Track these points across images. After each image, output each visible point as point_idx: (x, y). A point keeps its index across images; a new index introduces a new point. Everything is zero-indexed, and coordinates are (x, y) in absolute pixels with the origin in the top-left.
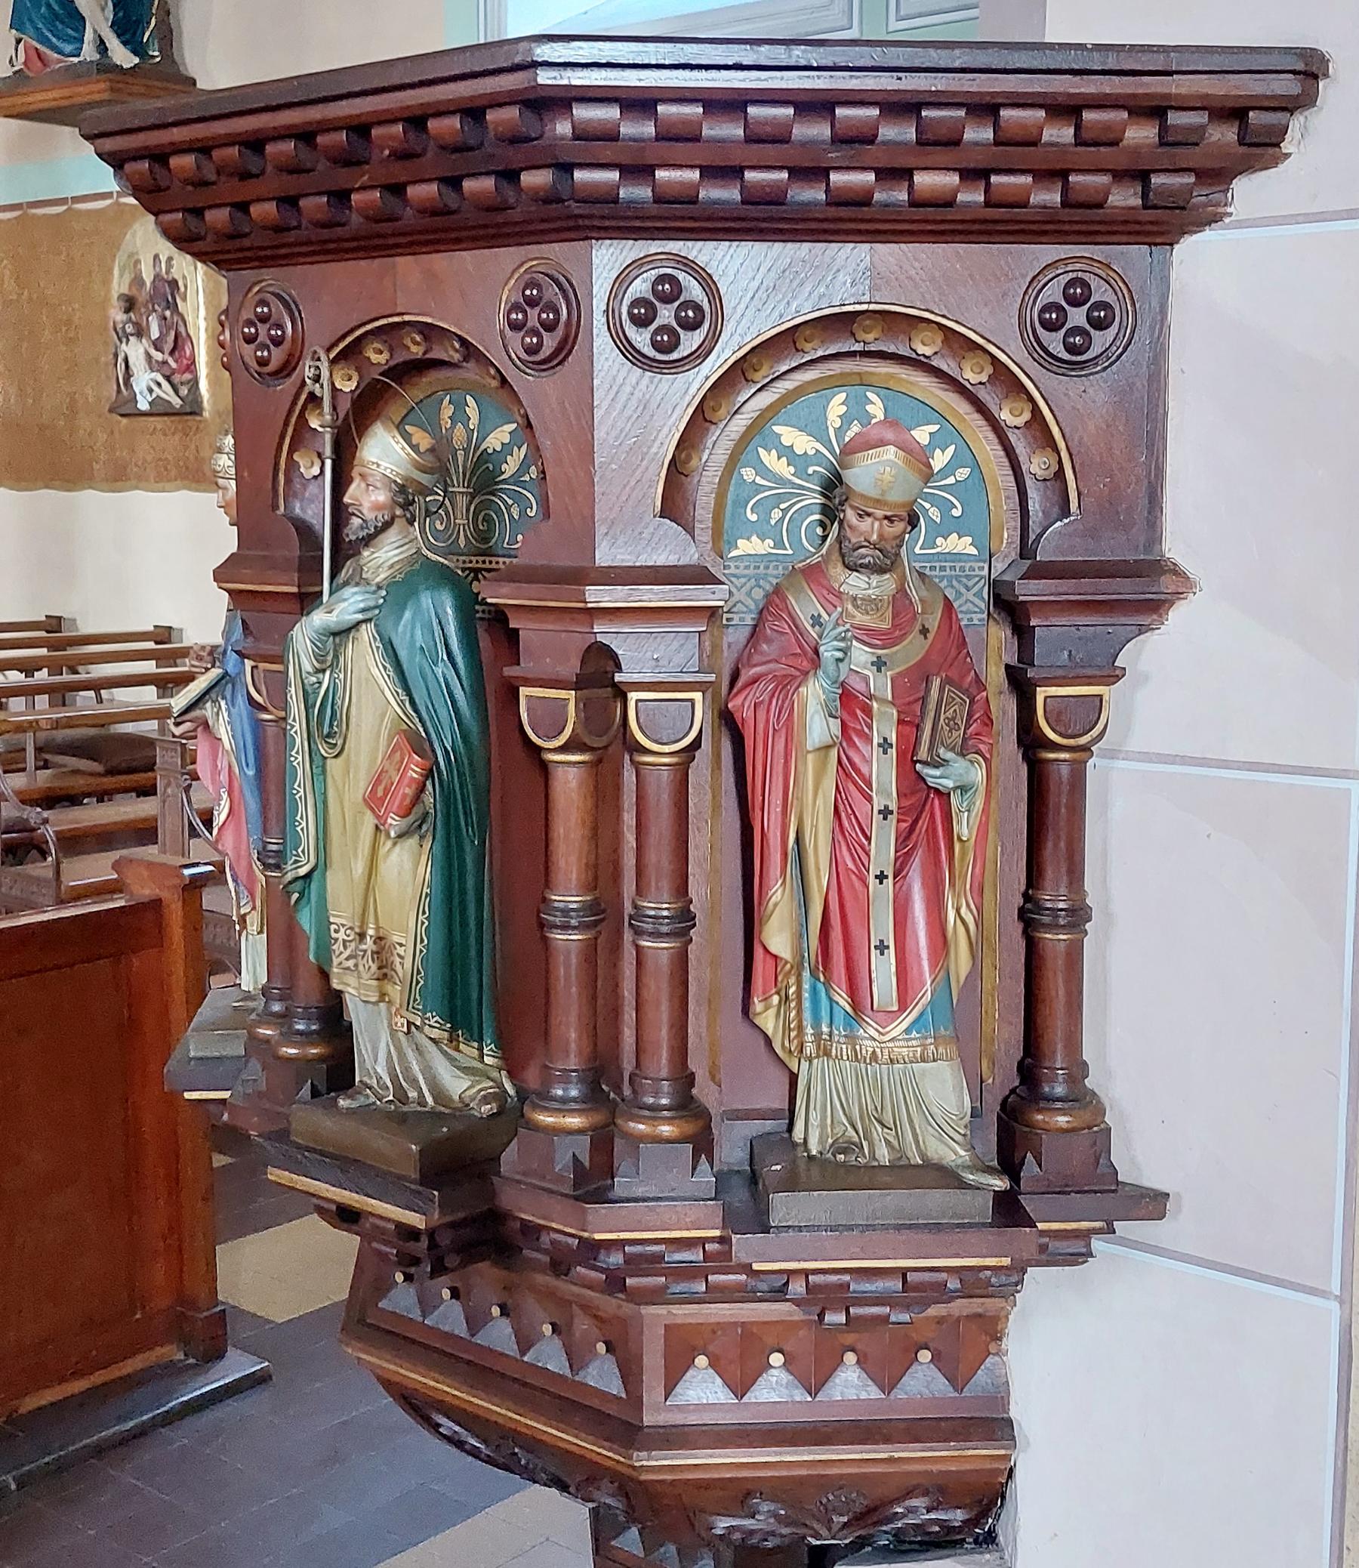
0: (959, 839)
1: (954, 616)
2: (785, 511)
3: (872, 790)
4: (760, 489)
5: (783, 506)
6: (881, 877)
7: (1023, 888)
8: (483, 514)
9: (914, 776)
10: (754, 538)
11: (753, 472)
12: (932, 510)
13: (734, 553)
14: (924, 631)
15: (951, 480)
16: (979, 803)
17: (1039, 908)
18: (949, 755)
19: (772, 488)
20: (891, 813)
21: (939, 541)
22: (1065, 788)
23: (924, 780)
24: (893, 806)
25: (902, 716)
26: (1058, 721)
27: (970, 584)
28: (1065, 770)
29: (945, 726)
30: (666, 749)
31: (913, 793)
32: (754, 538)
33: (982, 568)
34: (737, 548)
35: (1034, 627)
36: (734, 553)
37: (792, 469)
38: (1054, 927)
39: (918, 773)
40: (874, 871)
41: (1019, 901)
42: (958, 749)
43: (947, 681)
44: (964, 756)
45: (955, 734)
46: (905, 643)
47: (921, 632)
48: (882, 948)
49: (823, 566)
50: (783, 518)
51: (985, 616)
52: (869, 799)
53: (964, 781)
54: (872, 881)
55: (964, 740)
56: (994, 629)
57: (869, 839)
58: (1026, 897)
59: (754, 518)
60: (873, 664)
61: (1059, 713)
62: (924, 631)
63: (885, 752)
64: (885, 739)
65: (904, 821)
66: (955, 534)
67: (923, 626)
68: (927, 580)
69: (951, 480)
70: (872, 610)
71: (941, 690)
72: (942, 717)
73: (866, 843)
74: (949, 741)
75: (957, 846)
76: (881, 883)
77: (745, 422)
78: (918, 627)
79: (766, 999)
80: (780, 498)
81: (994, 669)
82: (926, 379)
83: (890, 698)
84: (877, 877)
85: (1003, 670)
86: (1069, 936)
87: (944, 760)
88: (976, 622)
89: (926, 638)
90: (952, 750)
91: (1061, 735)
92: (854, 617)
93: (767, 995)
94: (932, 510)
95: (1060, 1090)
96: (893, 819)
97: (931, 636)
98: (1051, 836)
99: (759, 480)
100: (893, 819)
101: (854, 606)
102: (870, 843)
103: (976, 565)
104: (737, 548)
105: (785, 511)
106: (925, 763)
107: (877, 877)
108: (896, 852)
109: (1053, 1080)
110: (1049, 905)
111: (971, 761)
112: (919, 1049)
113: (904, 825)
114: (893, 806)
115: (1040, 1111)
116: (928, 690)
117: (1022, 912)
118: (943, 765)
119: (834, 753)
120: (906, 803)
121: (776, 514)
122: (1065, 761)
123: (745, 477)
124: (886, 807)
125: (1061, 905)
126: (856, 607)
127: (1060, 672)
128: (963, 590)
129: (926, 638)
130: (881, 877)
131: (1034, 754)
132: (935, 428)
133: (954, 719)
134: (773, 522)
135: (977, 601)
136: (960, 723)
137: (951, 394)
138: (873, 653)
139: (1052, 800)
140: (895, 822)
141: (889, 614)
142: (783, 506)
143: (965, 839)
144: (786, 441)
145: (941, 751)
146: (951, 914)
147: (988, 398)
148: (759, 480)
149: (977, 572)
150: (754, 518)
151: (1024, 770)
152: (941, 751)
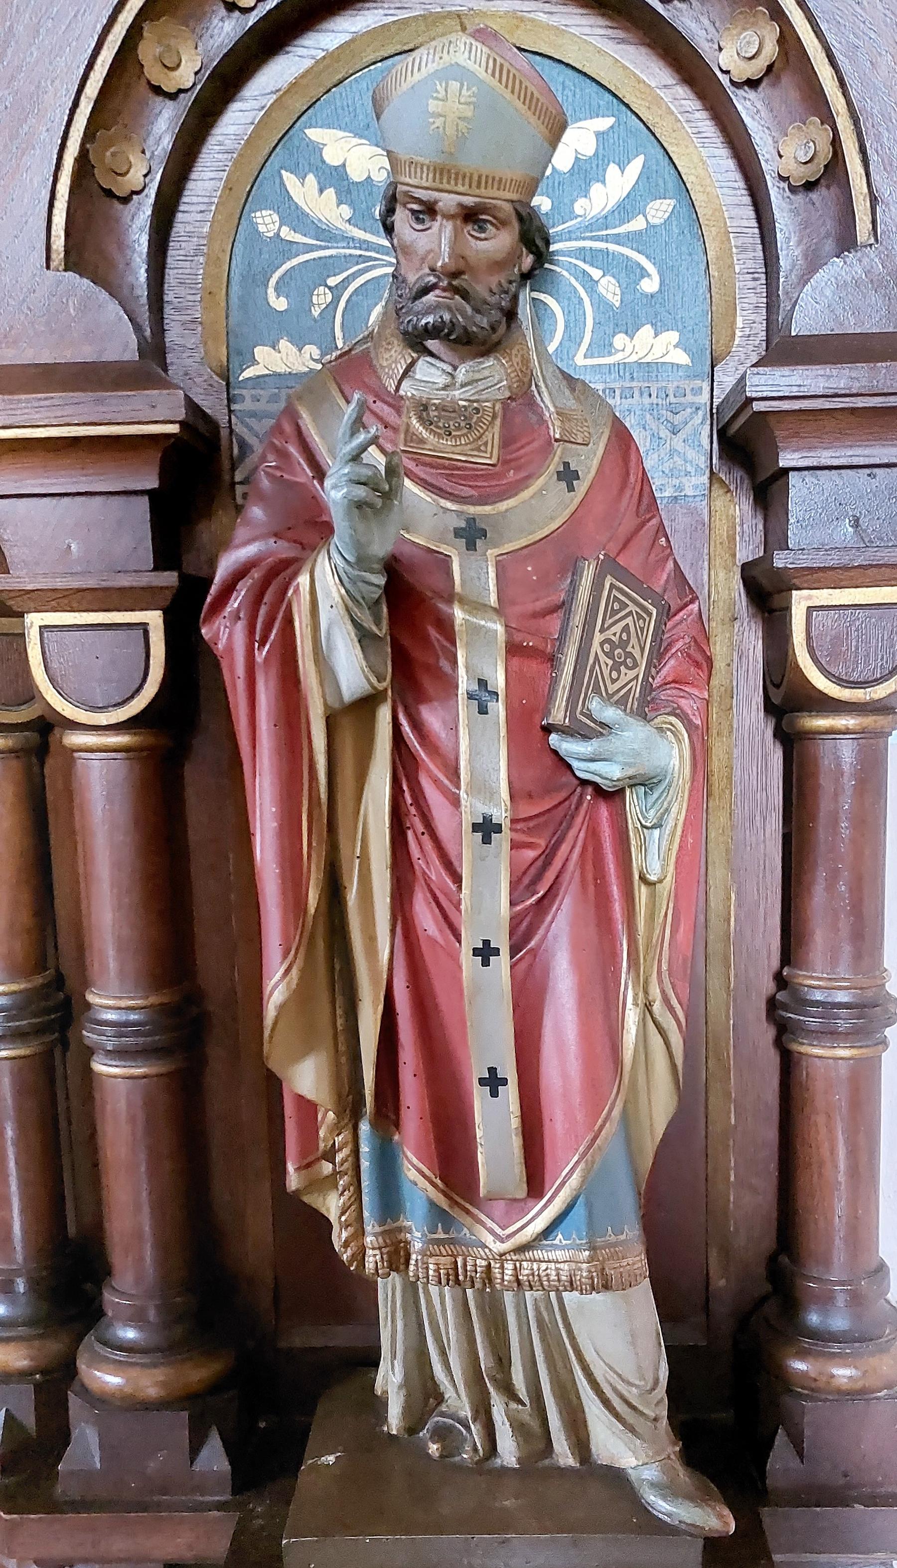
0: (643, 878)
1: (633, 457)
2: (337, 291)
3: (459, 788)
4: (288, 249)
5: (332, 281)
6: (486, 952)
7: (775, 963)
8: (578, 715)
9: (549, 760)
10: (284, 344)
11: (276, 217)
12: (604, 281)
13: (248, 373)
14: (568, 476)
15: (638, 224)
16: (678, 812)
17: (802, 1003)
18: (610, 714)
19: (310, 248)
20: (498, 829)
21: (620, 340)
22: (848, 783)
23: (569, 767)
24: (501, 814)
25: (518, 637)
26: (835, 654)
27: (677, 420)
28: (847, 751)
29: (602, 658)
30: (103, 719)
31: (547, 791)
32: (284, 344)
33: (698, 391)
34: (254, 362)
35: (786, 471)
36: (248, 373)
37: (346, 211)
38: (831, 1035)
39: (555, 752)
40: (470, 940)
41: (768, 986)
42: (633, 703)
43: (610, 566)
44: (645, 717)
45: (627, 675)
46: (525, 494)
47: (560, 476)
48: (493, 1082)
49: (372, 355)
50: (336, 300)
51: (705, 479)
52: (455, 802)
53: (644, 767)
54: (468, 962)
55: (647, 688)
56: (721, 501)
57: (457, 879)
58: (781, 981)
59: (280, 304)
60: (458, 533)
61: (837, 640)
62: (568, 476)
63: (483, 710)
64: (482, 683)
65: (530, 846)
66: (648, 327)
67: (566, 465)
68: (579, 386)
69: (638, 224)
70: (458, 428)
71: (598, 586)
72: (598, 638)
73: (453, 887)
74: (612, 688)
75: (642, 893)
76: (486, 963)
77: (248, 117)
78: (555, 465)
79: (308, 1166)
80: (328, 266)
81: (722, 575)
82: (584, 21)
83: (493, 600)
84: (476, 952)
85: (738, 576)
86: (854, 1052)
87: (603, 725)
88: (690, 492)
89: (571, 488)
90: (622, 703)
91: (840, 681)
92: (422, 441)
93: (311, 1158)
94: (604, 281)
95: (839, 1322)
96: (502, 841)
97: (581, 487)
98: (821, 875)
99: (286, 233)
100: (502, 841)
101: (420, 419)
102: (460, 888)
103: (687, 385)
104: (254, 362)
105: (337, 291)
106: (566, 731)
107: (476, 952)
108: (512, 904)
109: (826, 1300)
110: (818, 996)
111: (660, 730)
112: (565, 1266)
113: (531, 854)
114: (501, 814)
115: (803, 1354)
116: (573, 589)
117: (772, 1004)
118: (602, 734)
119: (384, 714)
120: (529, 810)
121: (322, 297)
122: (847, 731)
123: (262, 228)
124: (487, 819)
125: (842, 997)
126: (427, 422)
127: (833, 560)
128: (664, 433)
129: (571, 488)
130: (486, 952)
131: (791, 723)
132: (604, 123)
133: (623, 644)
134: (316, 312)
135: (691, 454)
136: (637, 653)
137: (631, 49)
138: (459, 513)
139: (825, 806)
140: (506, 846)
141: (494, 434)
142: (332, 281)
143: (653, 878)
144: (332, 157)
145: (595, 704)
146: (632, 1017)
147: (693, 25)
148: (286, 233)
149: (690, 398)
150: (280, 304)
151: (777, 756)
152: (595, 704)
